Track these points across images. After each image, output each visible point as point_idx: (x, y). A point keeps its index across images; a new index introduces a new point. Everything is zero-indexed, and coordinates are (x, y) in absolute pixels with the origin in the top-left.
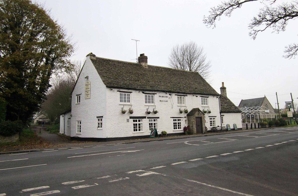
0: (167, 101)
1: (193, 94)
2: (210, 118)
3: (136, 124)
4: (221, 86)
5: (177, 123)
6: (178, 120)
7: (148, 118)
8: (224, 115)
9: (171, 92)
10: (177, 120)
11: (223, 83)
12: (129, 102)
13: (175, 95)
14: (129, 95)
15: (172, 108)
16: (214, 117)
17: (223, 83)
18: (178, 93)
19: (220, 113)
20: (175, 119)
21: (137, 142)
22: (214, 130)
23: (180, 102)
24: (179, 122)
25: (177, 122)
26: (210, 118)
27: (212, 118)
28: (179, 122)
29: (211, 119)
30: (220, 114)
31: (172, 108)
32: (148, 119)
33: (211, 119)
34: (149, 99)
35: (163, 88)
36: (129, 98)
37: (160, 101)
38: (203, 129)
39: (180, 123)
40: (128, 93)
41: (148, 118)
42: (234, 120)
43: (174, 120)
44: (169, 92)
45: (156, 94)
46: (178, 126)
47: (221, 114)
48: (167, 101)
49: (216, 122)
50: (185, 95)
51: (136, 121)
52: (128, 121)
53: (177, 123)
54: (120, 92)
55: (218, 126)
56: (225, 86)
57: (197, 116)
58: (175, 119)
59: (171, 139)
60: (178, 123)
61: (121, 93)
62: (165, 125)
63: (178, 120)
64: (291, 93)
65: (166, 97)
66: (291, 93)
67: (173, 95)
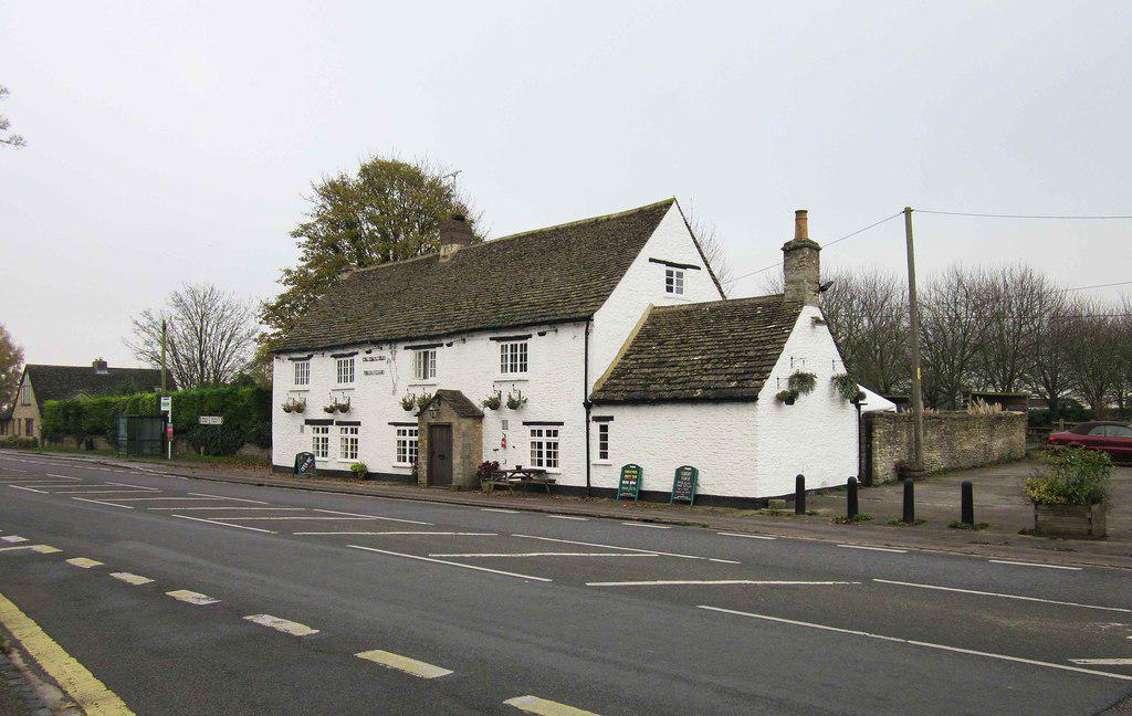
0: (382, 373)
1: (464, 336)
2: (399, 431)
3: (540, 445)
4: (790, 235)
5: (544, 445)
6: (549, 435)
7: (339, 423)
8: (611, 418)
9: (392, 341)
10: (544, 433)
11: (801, 215)
13: (406, 348)
17: (801, 215)
18: (411, 339)
19: (588, 406)
22: (537, 486)
23: (425, 368)
24: (552, 439)
25: (544, 439)
26: (399, 431)
27: (544, 429)
28: (552, 439)
29: (404, 435)
30: (584, 410)
32: (339, 428)
33: (404, 435)
34: (514, 358)
35: (394, 329)
37: (366, 373)
38: (455, 472)
39: (556, 445)
40: (523, 342)
42: (793, 440)
43: (533, 432)
45: (357, 353)
46: (549, 454)
47: (588, 414)
48: (382, 373)
49: (560, 450)
53: (544, 445)
54: (499, 339)
56: (813, 235)
57: (433, 421)
58: (402, 428)
60: (549, 445)
61: (504, 343)
62: (382, 452)
63: (549, 435)
64: (651, 260)
65: (381, 359)
66: (651, 260)
67: (400, 347)
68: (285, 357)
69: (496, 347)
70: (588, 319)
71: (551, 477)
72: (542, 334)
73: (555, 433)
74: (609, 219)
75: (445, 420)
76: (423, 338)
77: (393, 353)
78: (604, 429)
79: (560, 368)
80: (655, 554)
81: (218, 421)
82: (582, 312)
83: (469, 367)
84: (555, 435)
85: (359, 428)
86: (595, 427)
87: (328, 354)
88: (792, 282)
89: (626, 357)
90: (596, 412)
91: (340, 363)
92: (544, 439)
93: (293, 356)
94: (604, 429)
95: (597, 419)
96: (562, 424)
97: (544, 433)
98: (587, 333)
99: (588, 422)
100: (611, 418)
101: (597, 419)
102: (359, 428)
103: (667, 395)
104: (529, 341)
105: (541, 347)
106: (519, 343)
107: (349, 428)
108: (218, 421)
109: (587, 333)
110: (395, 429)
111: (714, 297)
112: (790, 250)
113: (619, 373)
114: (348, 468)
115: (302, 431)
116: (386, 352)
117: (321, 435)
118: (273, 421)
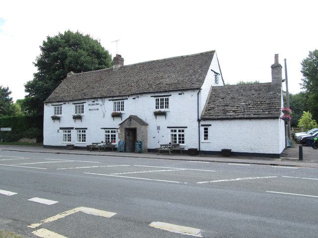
0: (98, 109)
3: (109, 136)
4: (273, 62)
8: (210, 125)
9: (102, 98)
10: (177, 131)
11: (276, 56)
12: (168, 108)
14: (168, 99)
15: (104, 116)
16: (112, 129)
17: (276, 56)
19: (199, 121)
20: (107, 130)
21: (219, 162)
25: (110, 134)
30: (197, 123)
31: (104, 116)
32: (76, 131)
34: (58, 111)
36: (168, 103)
37: (90, 110)
39: (183, 135)
40: (167, 97)
41: (76, 129)
43: (172, 131)
44: (101, 98)
47: (199, 123)
48: (98, 109)
50: (124, 98)
51: (175, 131)
52: (58, 131)
54: (54, 105)
55: (102, 142)
57: (128, 127)
58: (107, 130)
59: (219, 162)
60: (112, 136)
61: (115, 101)
63: (179, 131)
67: (107, 101)
68: (50, 104)
69: (74, 106)
70: (199, 89)
71: (183, 147)
72: (65, 104)
73: (85, 132)
74: (187, 56)
75: (133, 127)
76: (117, 96)
77: (104, 102)
78: (206, 129)
79: (185, 109)
80: (183, 169)
81: (10, 129)
82: (195, 86)
83: (141, 107)
84: (183, 131)
85: (86, 130)
86: (202, 129)
87: (71, 103)
88: (276, 78)
89: (209, 103)
90: (202, 123)
91: (76, 107)
92: (81, 133)
93: (54, 104)
94: (206, 129)
95: (202, 125)
96: (187, 127)
97: (177, 131)
98: (198, 94)
99: (199, 127)
100: (210, 125)
101: (202, 125)
102: (86, 130)
103: (236, 117)
104: (170, 98)
105: (175, 100)
106: (121, 101)
107: (67, 130)
108: (10, 129)
109: (198, 94)
110: (104, 130)
111: (222, 85)
112: (273, 67)
113: (208, 109)
114: (65, 145)
115: (58, 131)
116: (100, 102)
117: (67, 133)
118: (44, 128)
